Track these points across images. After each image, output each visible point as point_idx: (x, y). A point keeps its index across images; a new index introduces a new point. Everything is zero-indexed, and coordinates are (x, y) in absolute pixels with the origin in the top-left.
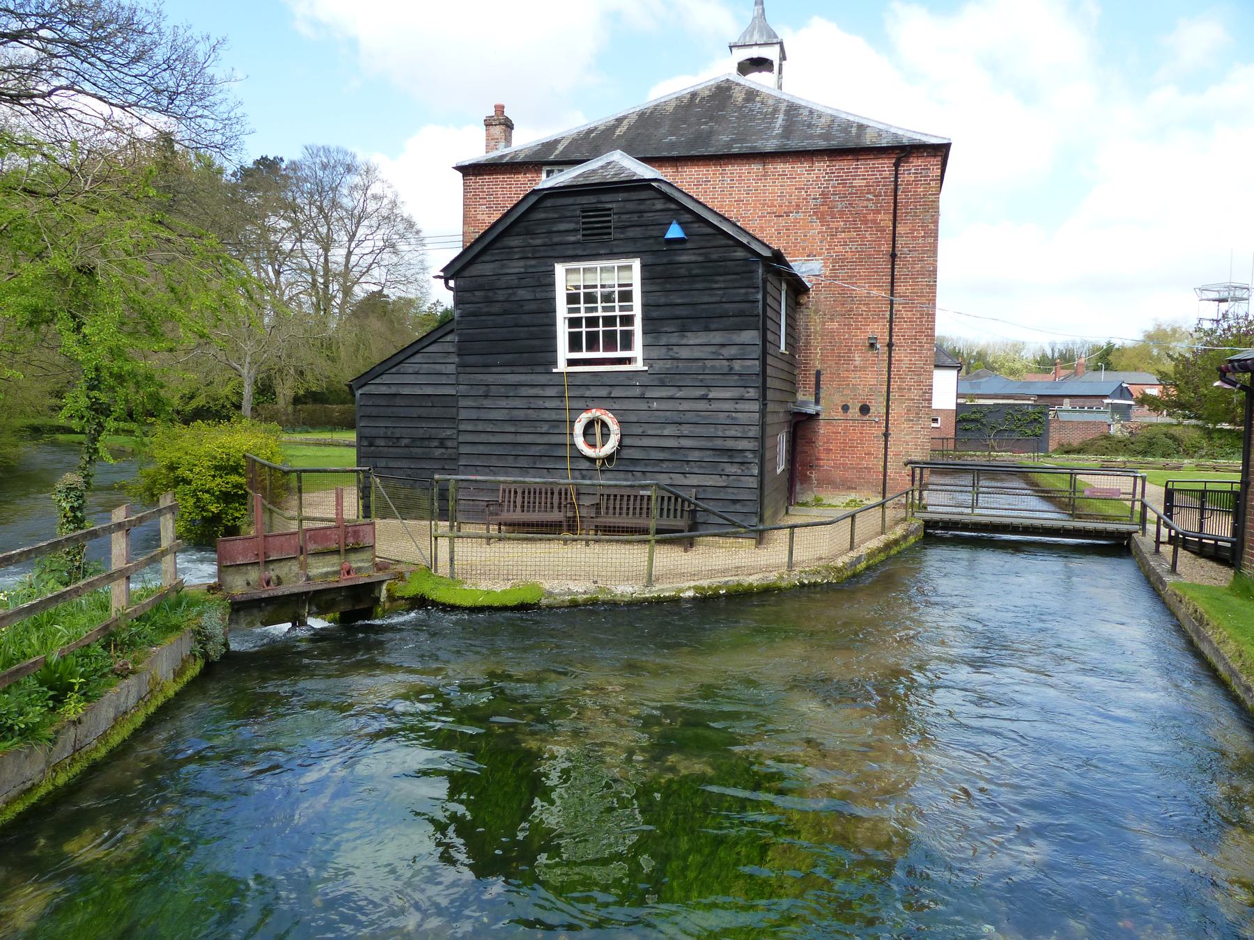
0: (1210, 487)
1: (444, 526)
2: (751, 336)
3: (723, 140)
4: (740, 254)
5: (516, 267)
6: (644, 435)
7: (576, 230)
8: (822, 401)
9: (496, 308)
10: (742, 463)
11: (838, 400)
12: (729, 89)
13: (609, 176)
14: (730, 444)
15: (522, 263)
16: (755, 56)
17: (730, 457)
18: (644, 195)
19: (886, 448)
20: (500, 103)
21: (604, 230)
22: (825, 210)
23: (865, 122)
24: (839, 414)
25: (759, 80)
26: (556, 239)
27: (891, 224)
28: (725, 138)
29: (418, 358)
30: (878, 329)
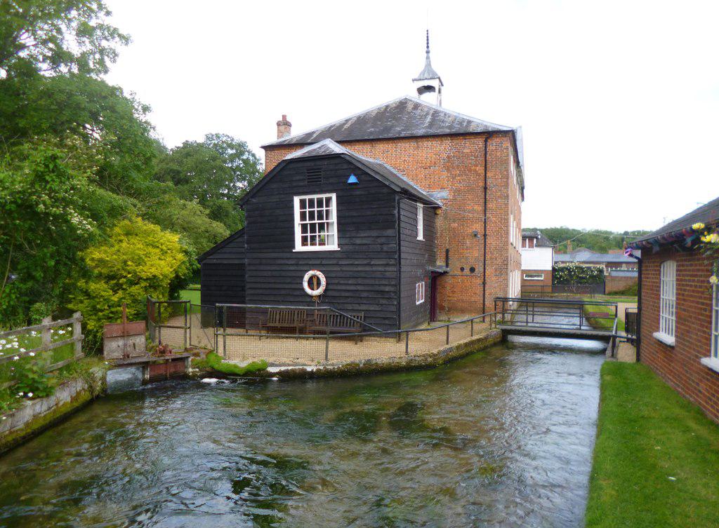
1: (221, 331)
3: (398, 130)
4: (385, 190)
7: (303, 180)
8: (450, 266)
11: (459, 265)
12: (406, 103)
13: (321, 152)
14: (382, 288)
15: (277, 196)
17: (382, 295)
18: (336, 161)
19: (484, 290)
20: (284, 114)
22: (449, 165)
23: (471, 119)
24: (459, 272)
25: (428, 99)
26: (295, 184)
28: (399, 129)
29: (231, 245)
30: (478, 227)
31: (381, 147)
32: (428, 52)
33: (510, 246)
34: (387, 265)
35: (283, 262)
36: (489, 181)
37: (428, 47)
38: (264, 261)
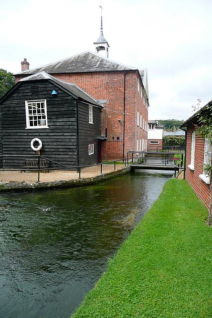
2: (73, 119)
5: (16, 101)
6: (48, 145)
9: (11, 112)
13: (38, 78)
20: (25, 58)
21: (37, 92)
22: (107, 87)
25: (102, 54)
26: (25, 94)
30: (121, 118)
31: (74, 78)
33: (136, 127)
35: (21, 134)
36: (126, 95)
37: (102, 26)
38: (11, 134)
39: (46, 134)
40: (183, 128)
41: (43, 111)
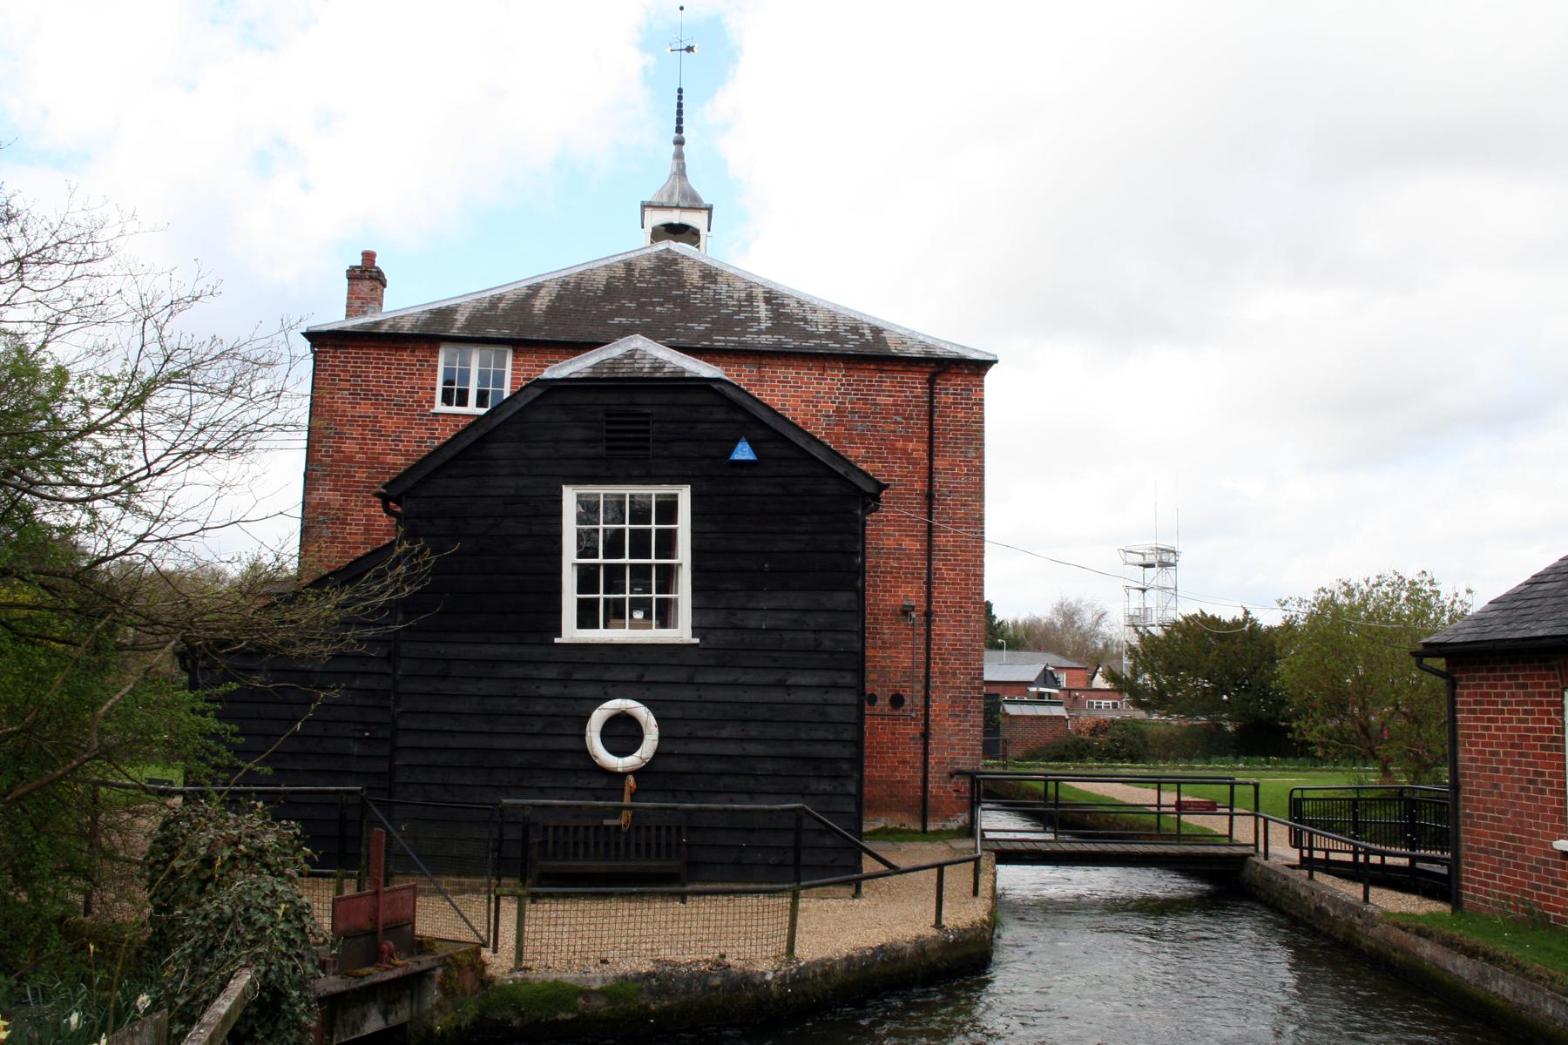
0: (1307, 794)
4: (833, 487)
6: (691, 737)
10: (836, 777)
16: (676, 221)
18: (698, 398)
19: (926, 754)
23: (877, 324)
27: (925, 455)
32: (680, 142)
34: (834, 686)
35: (518, 671)
36: (938, 479)
37: (679, 130)
39: (682, 675)
40: (1428, 661)
41: (667, 544)
